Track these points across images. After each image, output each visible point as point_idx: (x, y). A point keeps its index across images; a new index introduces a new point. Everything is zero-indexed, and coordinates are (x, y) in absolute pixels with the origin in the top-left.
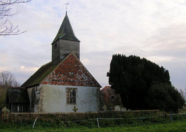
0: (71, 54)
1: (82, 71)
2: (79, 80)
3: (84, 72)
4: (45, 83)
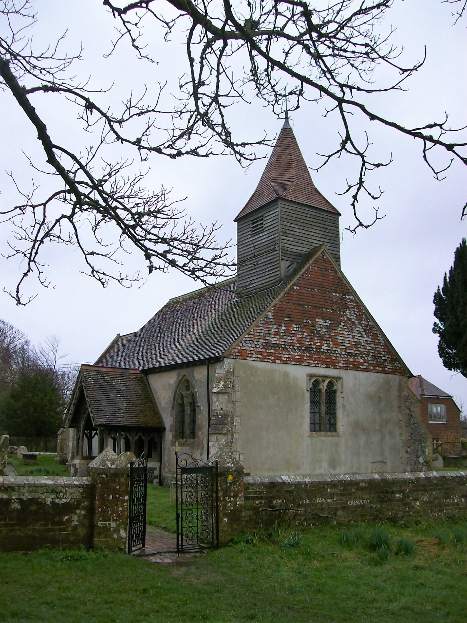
0: (319, 254)
1: (353, 318)
2: (347, 348)
3: (359, 318)
4: (243, 355)
